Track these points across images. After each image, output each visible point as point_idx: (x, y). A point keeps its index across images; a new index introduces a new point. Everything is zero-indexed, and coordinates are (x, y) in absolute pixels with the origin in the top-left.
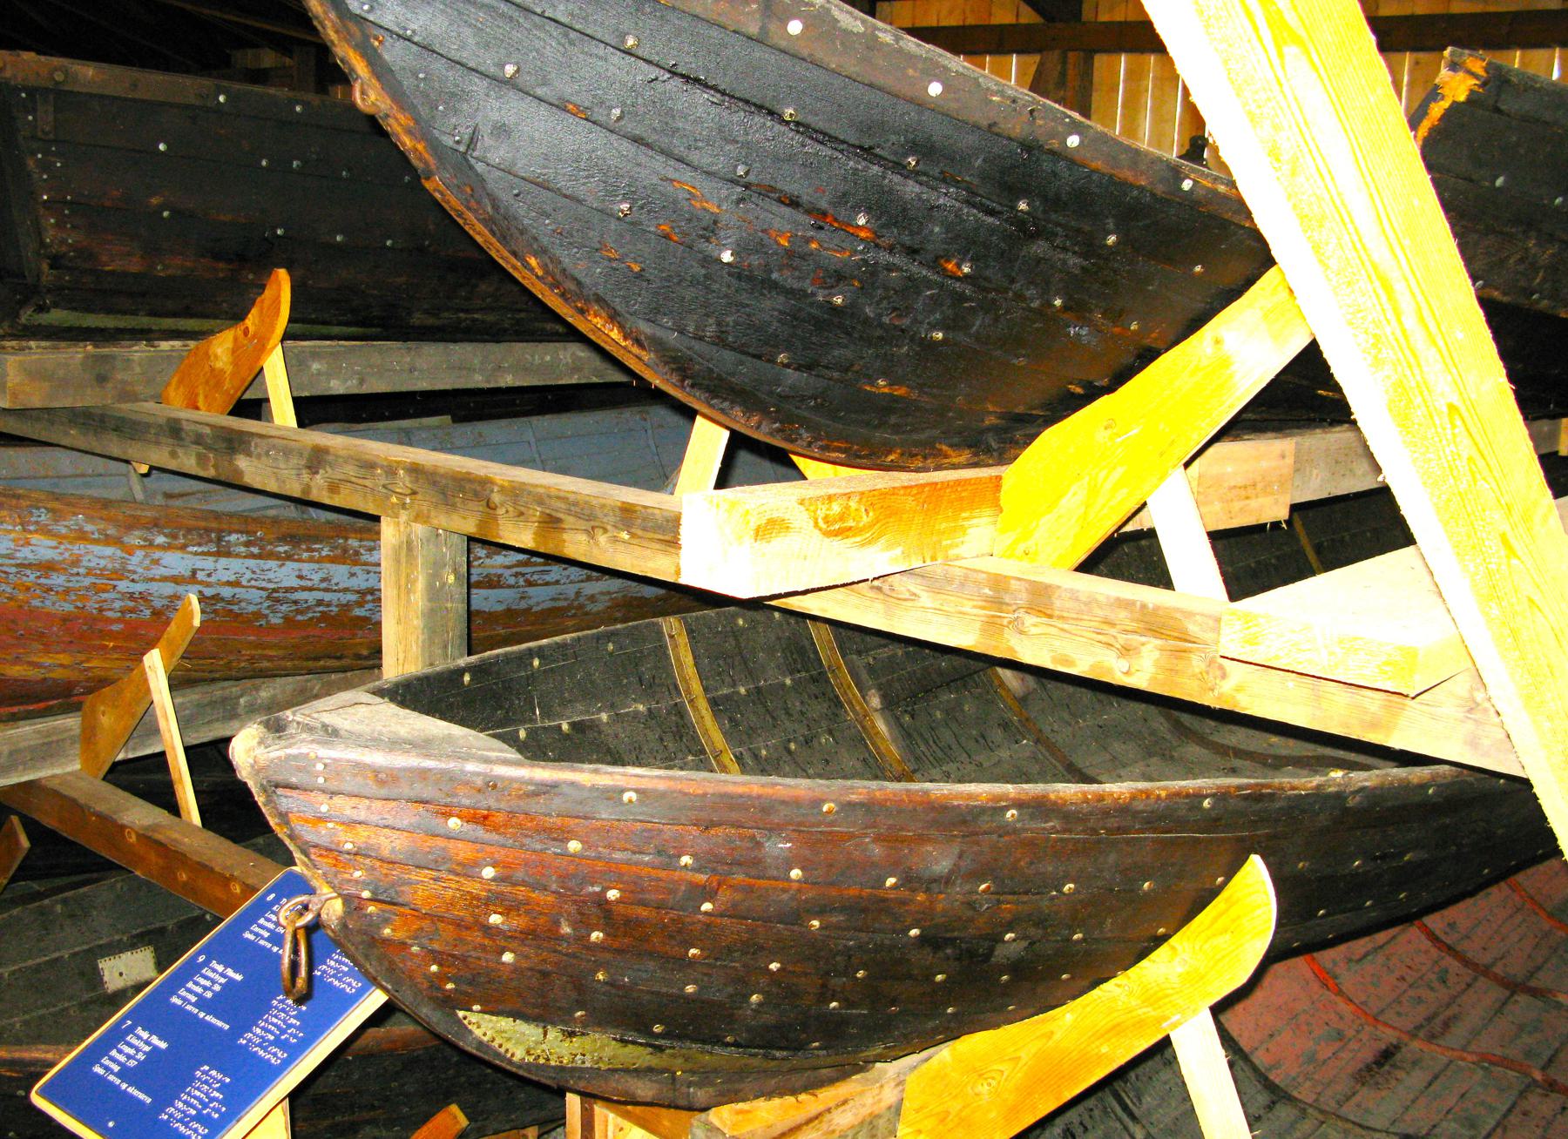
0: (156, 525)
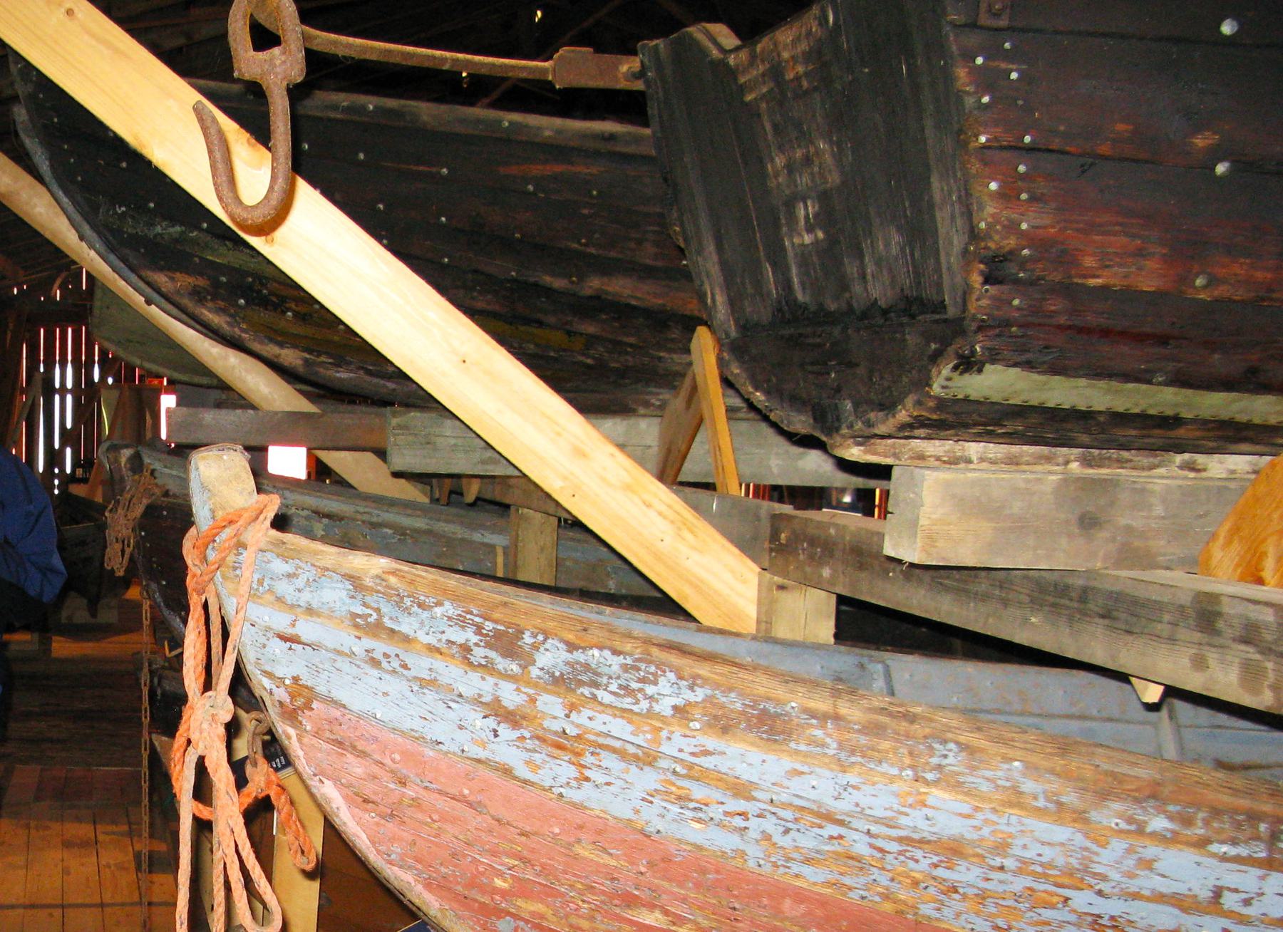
0: (1154, 796)
